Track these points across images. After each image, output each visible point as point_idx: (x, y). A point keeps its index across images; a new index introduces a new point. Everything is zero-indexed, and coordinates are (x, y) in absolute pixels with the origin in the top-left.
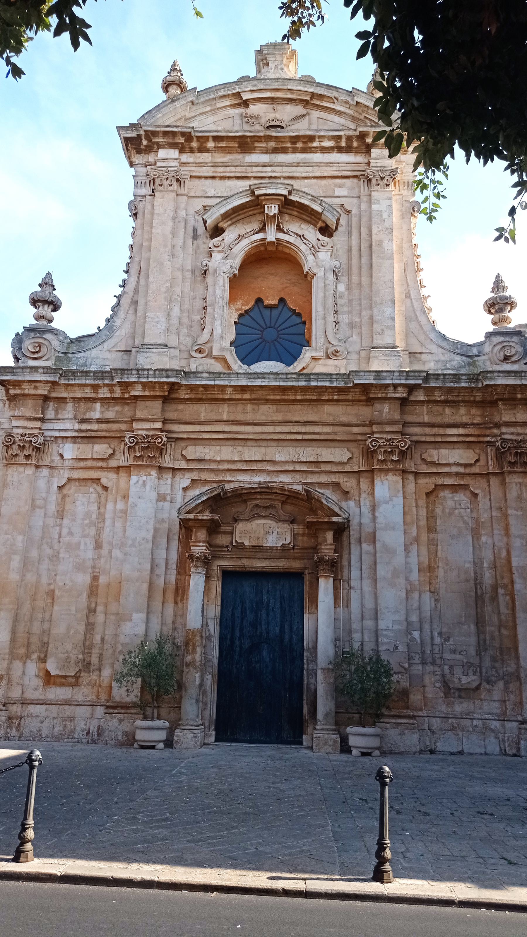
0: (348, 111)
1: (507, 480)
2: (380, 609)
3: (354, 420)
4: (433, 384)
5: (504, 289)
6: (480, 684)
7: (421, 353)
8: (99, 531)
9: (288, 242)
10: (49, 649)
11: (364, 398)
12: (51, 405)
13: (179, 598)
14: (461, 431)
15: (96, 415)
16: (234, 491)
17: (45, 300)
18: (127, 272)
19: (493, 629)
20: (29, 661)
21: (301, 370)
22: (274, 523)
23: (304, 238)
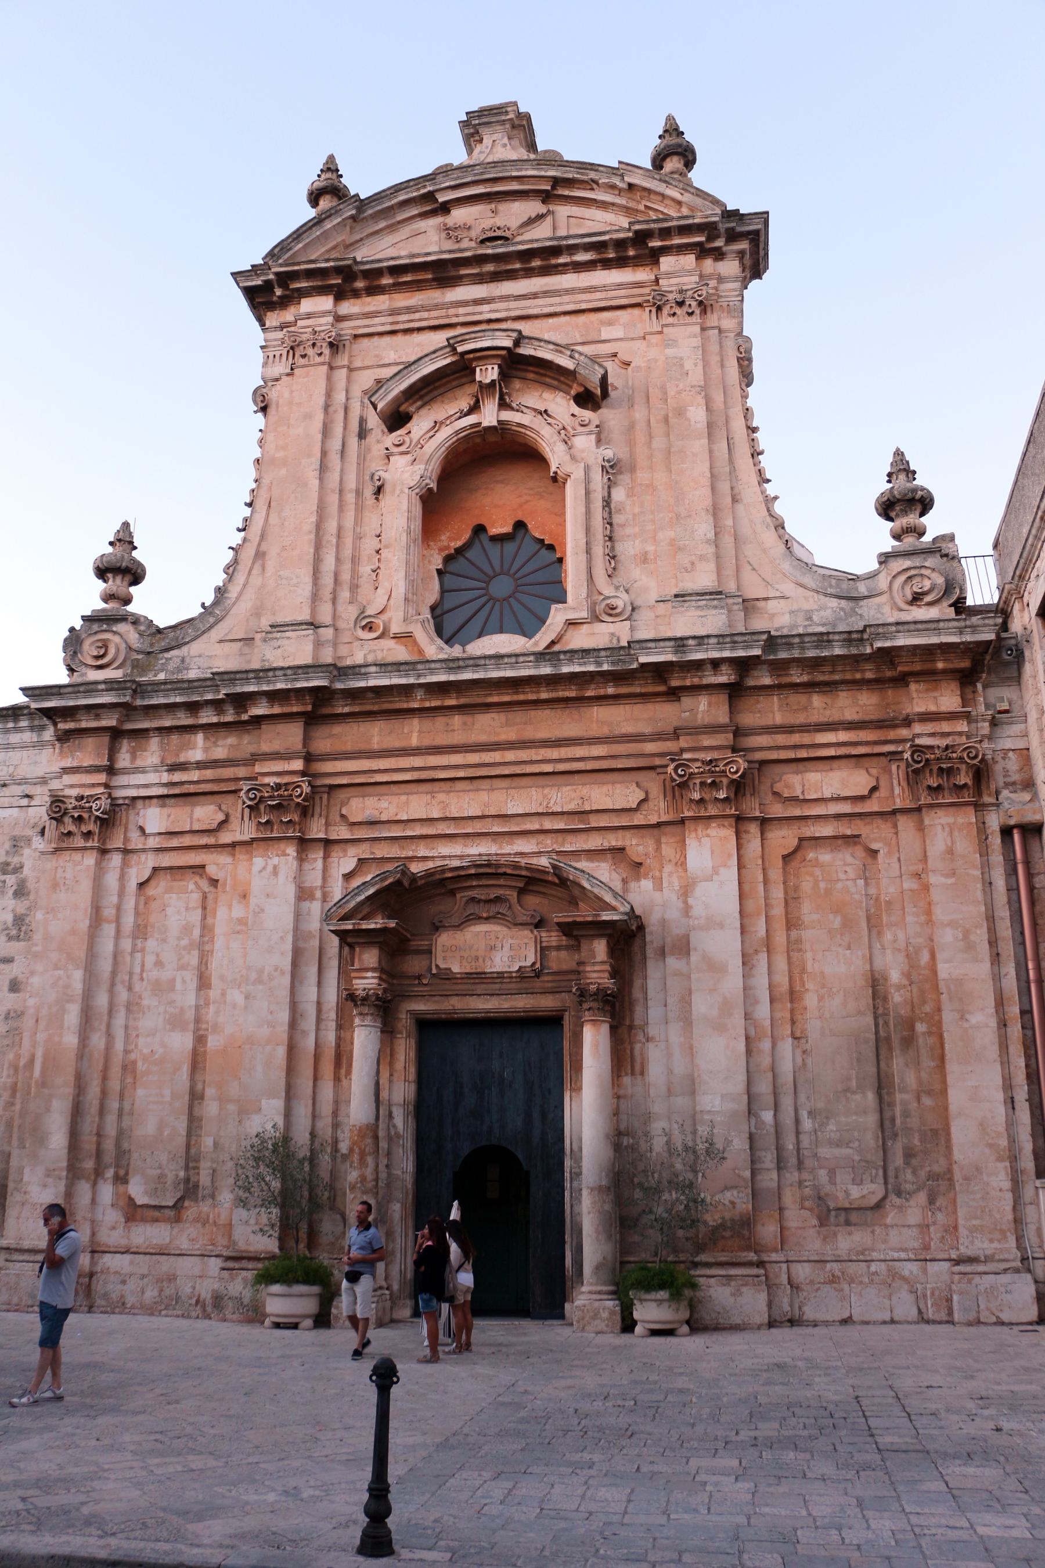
0: (618, 200)
1: (927, 822)
2: (699, 1076)
3: (647, 730)
4: (783, 655)
5: (911, 474)
6: (885, 1198)
7: (766, 599)
8: (204, 959)
9: (520, 425)
11: (662, 688)
12: (125, 745)
13: (343, 1071)
14: (843, 736)
15: (197, 755)
16: (429, 874)
17: (121, 570)
18: (250, 505)
19: (906, 1097)
20: (101, 1182)
21: (548, 647)
22: (505, 929)
23: (549, 415)
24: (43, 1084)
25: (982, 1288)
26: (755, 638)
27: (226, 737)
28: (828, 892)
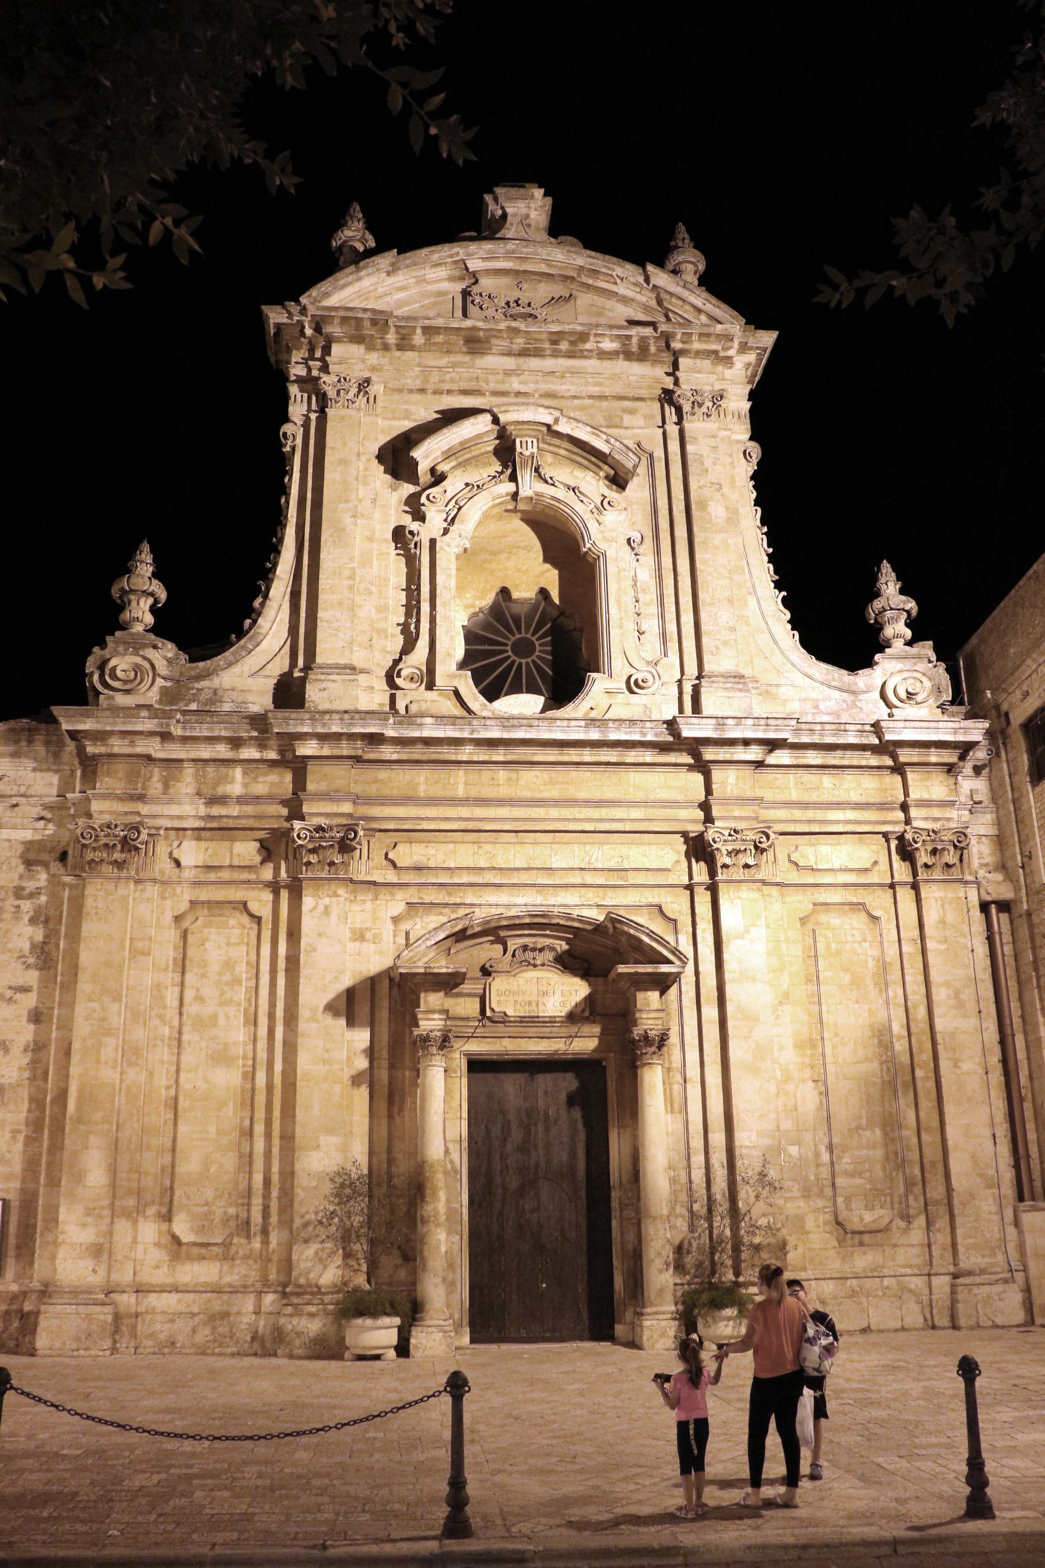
0: (638, 297)
7: (777, 685)
10: (176, 1198)
13: (396, 1109)
20: (141, 1219)
24: (79, 1120)
25: (980, 1298)
26: (786, 722)
27: (266, 775)
28: (838, 953)
